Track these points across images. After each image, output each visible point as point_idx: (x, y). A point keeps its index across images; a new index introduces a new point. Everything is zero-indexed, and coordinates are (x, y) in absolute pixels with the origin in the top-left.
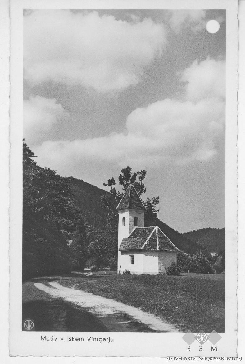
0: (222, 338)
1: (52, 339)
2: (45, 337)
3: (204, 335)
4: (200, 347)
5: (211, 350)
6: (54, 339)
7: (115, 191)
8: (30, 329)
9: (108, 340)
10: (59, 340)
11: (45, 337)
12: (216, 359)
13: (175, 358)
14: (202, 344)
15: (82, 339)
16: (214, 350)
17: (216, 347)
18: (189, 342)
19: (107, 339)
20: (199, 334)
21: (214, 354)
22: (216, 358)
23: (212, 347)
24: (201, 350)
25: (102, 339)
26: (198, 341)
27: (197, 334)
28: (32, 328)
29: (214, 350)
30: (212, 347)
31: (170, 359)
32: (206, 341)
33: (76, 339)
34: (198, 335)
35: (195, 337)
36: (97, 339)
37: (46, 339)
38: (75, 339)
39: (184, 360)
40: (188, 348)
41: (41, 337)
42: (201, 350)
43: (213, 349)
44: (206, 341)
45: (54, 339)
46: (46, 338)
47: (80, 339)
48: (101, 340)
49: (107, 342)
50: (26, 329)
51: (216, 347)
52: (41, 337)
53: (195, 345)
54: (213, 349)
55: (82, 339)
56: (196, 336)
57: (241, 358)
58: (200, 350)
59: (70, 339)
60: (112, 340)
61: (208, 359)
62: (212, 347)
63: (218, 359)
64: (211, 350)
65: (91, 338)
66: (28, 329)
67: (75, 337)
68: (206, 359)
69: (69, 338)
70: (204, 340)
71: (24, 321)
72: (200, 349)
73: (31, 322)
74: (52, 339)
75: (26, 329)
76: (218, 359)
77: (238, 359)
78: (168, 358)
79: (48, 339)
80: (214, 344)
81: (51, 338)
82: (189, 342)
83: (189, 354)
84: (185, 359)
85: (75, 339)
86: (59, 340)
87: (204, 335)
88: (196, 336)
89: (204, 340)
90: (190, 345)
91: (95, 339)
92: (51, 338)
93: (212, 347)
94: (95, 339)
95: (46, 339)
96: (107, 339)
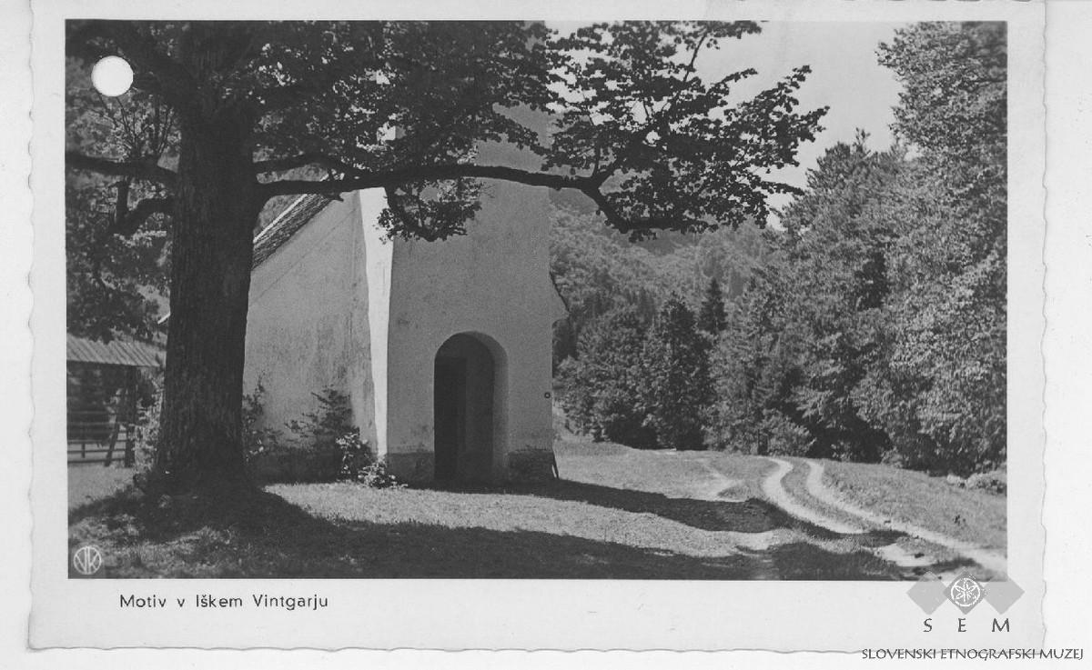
0: (1024, 595)
1: (152, 602)
2: (132, 597)
3: (971, 584)
4: (960, 620)
5: (993, 631)
6: (157, 602)
7: (672, 54)
8: (90, 573)
9: (312, 602)
10: (172, 604)
11: (132, 597)
12: (1008, 655)
13: (888, 654)
14: (966, 611)
15: (238, 602)
16: (1000, 630)
17: (1007, 622)
18: (929, 607)
19: (309, 600)
20: (956, 583)
21: (1001, 640)
22: (1008, 654)
23: (995, 620)
24: (962, 628)
25: (294, 600)
26: (953, 602)
27: (953, 584)
28: (96, 569)
29: (1000, 630)
30: (995, 621)
31: (873, 654)
32: (979, 601)
33: (220, 603)
34: (955, 586)
35: (947, 592)
36: (279, 601)
37: (135, 605)
38: (217, 603)
39: (914, 657)
40: (926, 624)
41: (122, 598)
42: (962, 628)
43: (999, 627)
44: (976, 604)
45: (157, 602)
46: (135, 600)
47: (233, 601)
48: (291, 602)
49: (308, 610)
50: (80, 571)
51: (1007, 622)
52: (122, 598)
53: (947, 613)
54: (999, 627)
55: (238, 602)
56: (949, 588)
57: (1079, 652)
58: (960, 630)
59: (207, 602)
60: (323, 603)
61: (983, 655)
62: (995, 621)
63: (1015, 656)
64: (993, 631)
65: (264, 598)
66: (86, 573)
67: (217, 597)
68: (978, 654)
69: (200, 598)
70: (971, 600)
71: (73, 550)
72: (960, 625)
73: (93, 554)
74: (152, 602)
75: (80, 571)
76: (1015, 656)
77: (1072, 655)
78: (867, 653)
79: (141, 603)
80: (1002, 610)
81: (149, 599)
82: (929, 607)
83: (926, 642)
84: (917, 655)
85: (217, 603)
86: (172, 604)
87: (971, 584)
88: (949, 588)
89: (971, 600)
90: (930, 613)
91: (274, 601)
92: (149, 599)
93: (995, 620)
94: (274, 601)
95: (135, 605)
96: (309, 600)
